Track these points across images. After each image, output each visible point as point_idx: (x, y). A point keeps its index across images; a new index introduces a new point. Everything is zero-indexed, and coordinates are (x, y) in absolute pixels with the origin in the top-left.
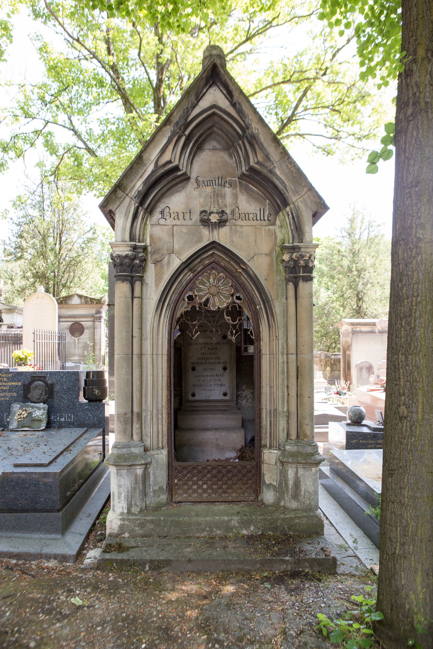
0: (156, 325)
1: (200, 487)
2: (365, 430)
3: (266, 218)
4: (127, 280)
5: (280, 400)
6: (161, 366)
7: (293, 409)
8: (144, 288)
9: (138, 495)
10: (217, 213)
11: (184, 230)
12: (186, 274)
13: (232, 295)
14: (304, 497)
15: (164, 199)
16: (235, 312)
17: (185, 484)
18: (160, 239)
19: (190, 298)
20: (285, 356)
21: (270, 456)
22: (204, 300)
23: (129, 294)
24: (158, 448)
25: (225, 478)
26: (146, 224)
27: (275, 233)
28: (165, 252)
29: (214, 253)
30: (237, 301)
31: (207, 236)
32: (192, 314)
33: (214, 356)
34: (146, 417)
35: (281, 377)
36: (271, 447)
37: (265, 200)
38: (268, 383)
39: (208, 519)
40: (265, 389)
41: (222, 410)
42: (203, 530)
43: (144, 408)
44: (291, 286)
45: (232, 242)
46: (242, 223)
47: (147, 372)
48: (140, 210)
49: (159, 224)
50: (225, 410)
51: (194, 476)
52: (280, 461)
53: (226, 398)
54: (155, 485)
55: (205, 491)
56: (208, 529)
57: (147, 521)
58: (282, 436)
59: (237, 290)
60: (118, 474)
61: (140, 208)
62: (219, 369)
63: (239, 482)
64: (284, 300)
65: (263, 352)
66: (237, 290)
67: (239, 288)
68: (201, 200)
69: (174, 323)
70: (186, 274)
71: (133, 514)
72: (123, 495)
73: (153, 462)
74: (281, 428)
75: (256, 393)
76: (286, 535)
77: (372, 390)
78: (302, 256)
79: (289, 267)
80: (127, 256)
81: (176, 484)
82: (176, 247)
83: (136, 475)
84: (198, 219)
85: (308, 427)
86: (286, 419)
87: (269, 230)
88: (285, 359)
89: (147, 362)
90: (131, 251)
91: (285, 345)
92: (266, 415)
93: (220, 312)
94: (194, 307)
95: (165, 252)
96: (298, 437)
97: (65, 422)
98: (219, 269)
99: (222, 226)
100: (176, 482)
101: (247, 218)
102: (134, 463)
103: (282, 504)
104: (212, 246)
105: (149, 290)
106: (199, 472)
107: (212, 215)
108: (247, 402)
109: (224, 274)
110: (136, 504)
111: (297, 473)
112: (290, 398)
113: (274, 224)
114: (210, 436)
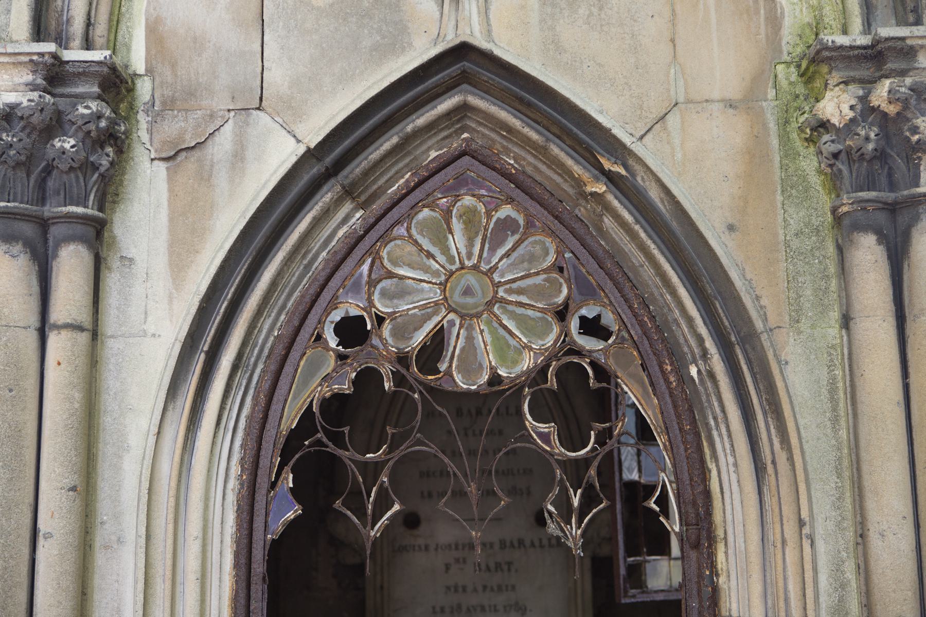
8: (112, 281)
12: (326, 214)
13: (562, 314)
16: (578, 394)
18: (198, 43)
19: (353, 332)
22: (419, 337)
28: (221, 103)
29: (463, 109)
33: (500, 599)
44: (868, 253)
45: (553, 47)
64: (833, 332)
66: (587, 291)
67: (596, 276)
69: (271, 458)
70: (326, 214)
79: (851, 156)
90: (33, 87)
91: (850, 573)
93: (499, 398)
94: (367, 378)
105: (138, 289)
109: (519, 207)
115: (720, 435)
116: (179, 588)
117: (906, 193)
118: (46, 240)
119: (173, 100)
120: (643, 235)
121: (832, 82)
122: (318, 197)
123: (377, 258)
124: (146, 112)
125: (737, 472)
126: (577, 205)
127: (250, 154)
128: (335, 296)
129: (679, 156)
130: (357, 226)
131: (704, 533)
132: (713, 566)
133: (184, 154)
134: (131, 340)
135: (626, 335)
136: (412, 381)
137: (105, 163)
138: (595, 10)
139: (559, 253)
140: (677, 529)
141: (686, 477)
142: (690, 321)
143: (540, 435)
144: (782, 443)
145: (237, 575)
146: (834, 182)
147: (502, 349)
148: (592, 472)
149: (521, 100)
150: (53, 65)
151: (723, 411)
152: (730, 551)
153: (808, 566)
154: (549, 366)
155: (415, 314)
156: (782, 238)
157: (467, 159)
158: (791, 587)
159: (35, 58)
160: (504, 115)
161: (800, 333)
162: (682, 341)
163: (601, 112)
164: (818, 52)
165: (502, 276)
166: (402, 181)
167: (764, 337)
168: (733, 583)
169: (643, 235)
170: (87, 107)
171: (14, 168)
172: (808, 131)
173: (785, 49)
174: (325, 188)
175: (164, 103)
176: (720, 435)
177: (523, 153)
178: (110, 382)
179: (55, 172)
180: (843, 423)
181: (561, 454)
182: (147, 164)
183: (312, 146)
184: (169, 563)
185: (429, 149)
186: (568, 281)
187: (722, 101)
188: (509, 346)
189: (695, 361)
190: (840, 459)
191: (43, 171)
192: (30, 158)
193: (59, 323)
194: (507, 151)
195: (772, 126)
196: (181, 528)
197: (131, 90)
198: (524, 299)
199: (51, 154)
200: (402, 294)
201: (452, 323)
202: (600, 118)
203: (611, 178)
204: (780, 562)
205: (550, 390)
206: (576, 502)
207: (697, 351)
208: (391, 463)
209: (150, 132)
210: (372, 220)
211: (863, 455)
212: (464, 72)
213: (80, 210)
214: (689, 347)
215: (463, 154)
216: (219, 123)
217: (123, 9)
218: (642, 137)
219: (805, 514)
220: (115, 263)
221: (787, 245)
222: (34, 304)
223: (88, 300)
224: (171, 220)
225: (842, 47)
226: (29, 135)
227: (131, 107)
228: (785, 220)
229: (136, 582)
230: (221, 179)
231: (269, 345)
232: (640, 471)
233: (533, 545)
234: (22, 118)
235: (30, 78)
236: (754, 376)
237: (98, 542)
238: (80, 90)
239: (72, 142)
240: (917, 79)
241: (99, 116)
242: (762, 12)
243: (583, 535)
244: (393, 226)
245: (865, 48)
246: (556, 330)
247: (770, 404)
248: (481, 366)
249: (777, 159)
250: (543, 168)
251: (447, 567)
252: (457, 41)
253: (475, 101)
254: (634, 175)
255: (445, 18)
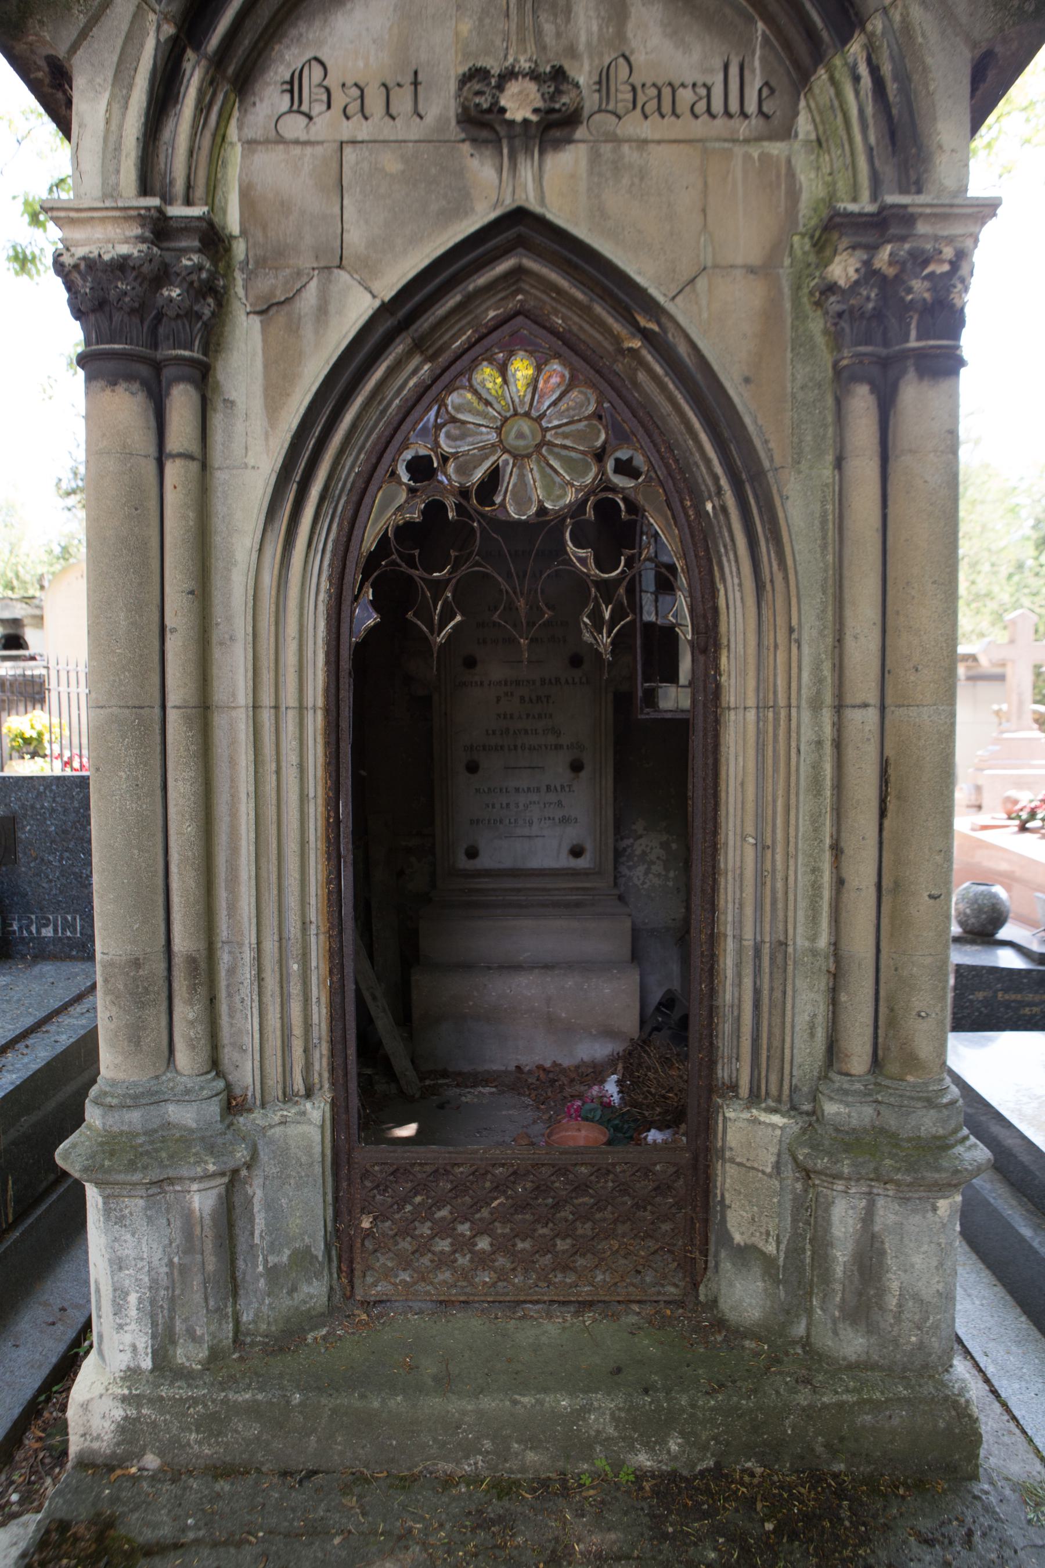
0: (268, 579)
1: (464, 1245)
2: (1008, 959)
3: (751, 107)
4: (129, 378)
5: (803, 904)
6: (294, 759)
7: (860, 943)
8: (217, 420)
9: (198, 1297)
10: (534, 76)
11: (391, 163)
13: (600, 456)
14: (898, 1317)
15: (302, 26)
16: (611, 525)
17: (406, 1231)
18: (285, 207)
19: (422, 469)
20: (827, 716)
21: (752, 1135)
22: (478, 474)
23: (143, 441)
24: (288, 1097)
25: (566, 1213)
26: (220, 139)
27: (791, 174)
28: (306, 262)
29: (518, 272)
30: (621, 481)
31: (490, 187)
32: (429, 535)
34: (232, 971)
35: (805, 805)
36: (755, 1098)
37: (751, 21)
38: (750, 829)
39: (488, 1403)
40: (737, 855)
41: (568, 905)
42: (469, 1450)
43: (223, 931)
44: (862, 401)
45: (599, 213)
46: (645, 129)
47: (233, 780)
48: (187, 66)
49: (280, 140)
50: (578, 905)
51: (439, 1204)
52: (798, 1165)
53: (582, 863)
54: (273, 1248)
55: (482, 1261)
56: (487, 1444)
57: (236, 1409)
58: (804, 1052)
59: (620, 435)
60: (113, 1216)
61: (190, 54)
62: (557, 768)
63: (621, 1229)
64: (827, 472)
65: (730, 696)
66: (620, 435)
68: (466, 27)
69: (354, 575)
71: (182, 1374)
72: (133, 1298)
73: (264, 1156)
74: (802, 1020)
75: (697, 869)
76: (816, 1478)
77: (985, 828)
78: (921, 259)
79: (852, 315)
80: (121, 266)
81: (369, 1234)
82: (356, 237)
83: (188, 1216)
84: (452, 110)
85: (923, 1026)
86: (823, 983)
87: (765, 157)
88: (828, 731)
89: (233, 743)
90: (141, 239)
91: (827, 672)
92: (739, 965)
93: (545, 527)
94: (435, 509)
95: (306, 262)
96: (876, 1063)
97: (56, 940)
98: (546, 341)
99: (558, 144)
100: (366, 1224)
101: (667, 107)
102: (171, 1173)
103: (800, 1329)
104: (511, 234)
105: (239, 427)
106: (460, 1188)
107: (513, 87)
108: (647, 872)
110: (191, 1333)
111: (868, 1217)
112: (849, 896)
113: (787, 132)
114: (525, 989)
115: (729, 561)
116: (281, 679)
117: (897, 348)
118: (160, 382)
119: (265, 259)
120: (671, 386)
121: (841, 247)
122: (391, 348)
123: (443, 404)
124: (242, 270)
125: (741, 591)
126: (615, 361)
127: (332, 309)
128: (407, 438)
129: (705, 315)
130: (426, 377)
131: (711, 641)
132: (717, 668)
133: (275, 309)
134: (234, 472)
135: (653, 475)
136: (472, 512)
137: (207, 312)
138: (636, 181)
139: (599, 403)
140: (689, 637)
141: (698, 595)
142: (708, 462)
143: (579, 559)
144: (779, 565)
145: (328, 671)
146: (836, 339)
147: (549, 487)
148: (622, 591)
149: (569, 262)
150: (158, 219)
151: (733, 540)
152: (732, 656)
153: (794, 665)
154: (587, 500)
155: (474, 455)
156: (789, 390)
157: (520, 319)
158: (779, 682)
159: (143, 212)
160: (554, 276)
161: (800, 472)
162: (700, 480)
163: (639, 274)
164: (831, 218)
165: (550, 422)
166: (464, 338)
167: (770, 475)
168: (733, 681)
169: (671, 386)
170: (190, 259)
171: (129, 314)
172: (817, 294)
173: (801, 221)
174: (398, 341)
175: (257, 263)
176: (729, 561)
177: (569, 314)
178: (219, 507)
179: (165, 319)
180: (830, 549)
181: (596, 575)
182: (243, 317)
183: (387, 299)
184: (272, 657)
185: (487, 309)
186: (606, 427)
187: (743, 267)
188: (554, 483)
189: (710, 498)
190: (825, 579)
191: (155, 318)
192: (142, 305)
193: (174, 452)
194: (556, 312)
195: (787, 291)
196: (281, 630)
197: (228, 250)
198: (568, 443)
199: (160, 302)
200: (462, 437)
201: (506, 462)
202: (639, 279)
203: (646, 335)
204: (771, 662)
205: (588, 521)
206: (607, 616)
207: (712, 489)
208: (454, 581)
209: (246, 288)
210: (438, 371)
211: (846, 573)
212: (519, 236)
213: (187, 353)
214: (707, 486)
215: (517, 313)
216: (305, 279)
217: (219, 175)
218: (673, 298)
219: (794, 623)
220: (220, 406)
221: (793, 396)
222: (152, 436)
223: (196, 434)
224: (266, 366)
225: (851, 214)
226: (141, 285)
227: (229, 266)
228: (793, 375)
229: (246, 671)
230: (308, 331)
231: (351, 480)
232: (657, 614)
233: (567, 682)
234: (134, 268)
235: (138, 231)
236: (759, 508)
237: (215, 639)
238: (183, 244)
239: (178, 291)
240: (915, 244)
241: (200, 268)
242: (783, 186)
243: (612, 643)
244: (456, 377)
245: (871, 215)
246: (594, 469)
247: (771, 533)
248: (530, 499)
249: (789, 321)
250: (586, 327)
251: (498, 699)
252: (514, 206)
253: (530, 264)
254: (665, 332)
255: (504, 184)
